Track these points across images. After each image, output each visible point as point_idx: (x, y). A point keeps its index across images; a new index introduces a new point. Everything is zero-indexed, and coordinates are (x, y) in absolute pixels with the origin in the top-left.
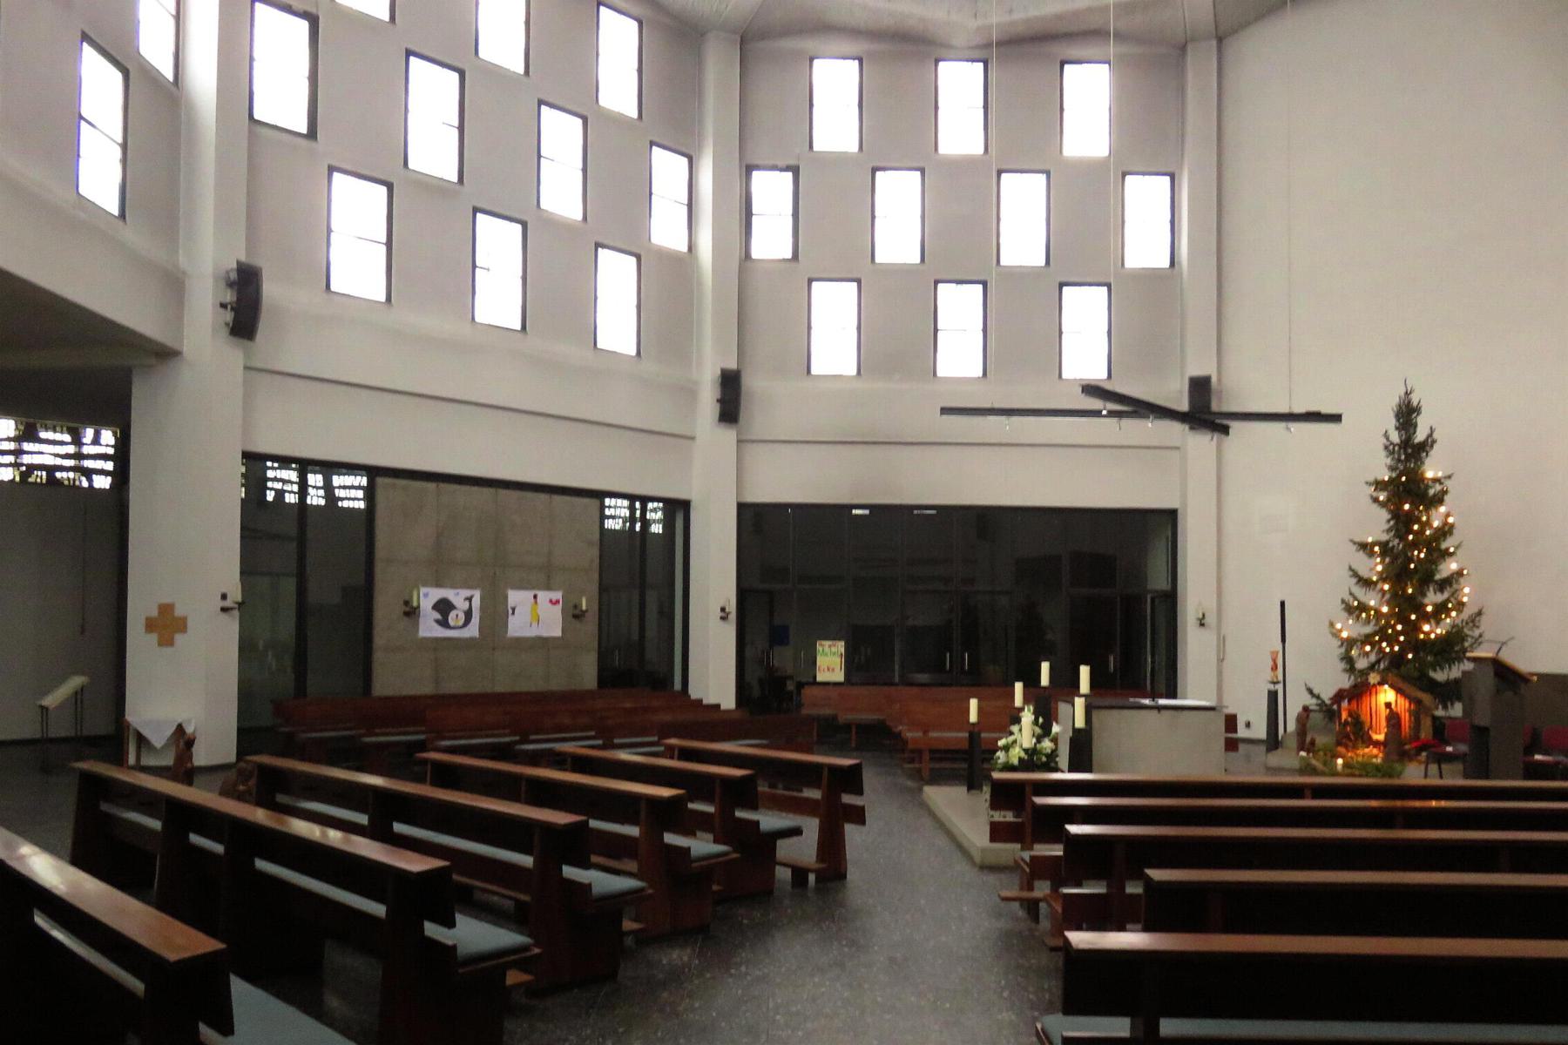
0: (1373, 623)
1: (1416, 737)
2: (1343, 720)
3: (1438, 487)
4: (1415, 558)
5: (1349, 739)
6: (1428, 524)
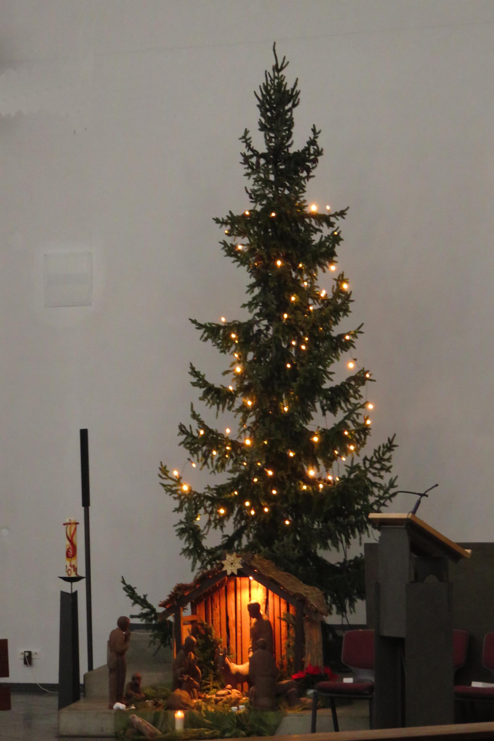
0: (230, 466)
1: (298, 663)
2: (184, 642)
3: (326, 231)
4: (293, 352)
5: (195, 674)
6: (312, 293)
